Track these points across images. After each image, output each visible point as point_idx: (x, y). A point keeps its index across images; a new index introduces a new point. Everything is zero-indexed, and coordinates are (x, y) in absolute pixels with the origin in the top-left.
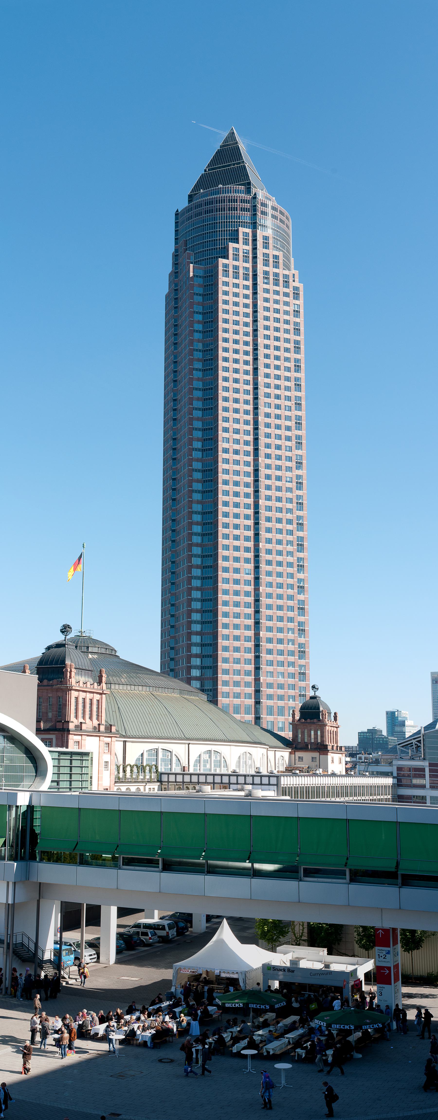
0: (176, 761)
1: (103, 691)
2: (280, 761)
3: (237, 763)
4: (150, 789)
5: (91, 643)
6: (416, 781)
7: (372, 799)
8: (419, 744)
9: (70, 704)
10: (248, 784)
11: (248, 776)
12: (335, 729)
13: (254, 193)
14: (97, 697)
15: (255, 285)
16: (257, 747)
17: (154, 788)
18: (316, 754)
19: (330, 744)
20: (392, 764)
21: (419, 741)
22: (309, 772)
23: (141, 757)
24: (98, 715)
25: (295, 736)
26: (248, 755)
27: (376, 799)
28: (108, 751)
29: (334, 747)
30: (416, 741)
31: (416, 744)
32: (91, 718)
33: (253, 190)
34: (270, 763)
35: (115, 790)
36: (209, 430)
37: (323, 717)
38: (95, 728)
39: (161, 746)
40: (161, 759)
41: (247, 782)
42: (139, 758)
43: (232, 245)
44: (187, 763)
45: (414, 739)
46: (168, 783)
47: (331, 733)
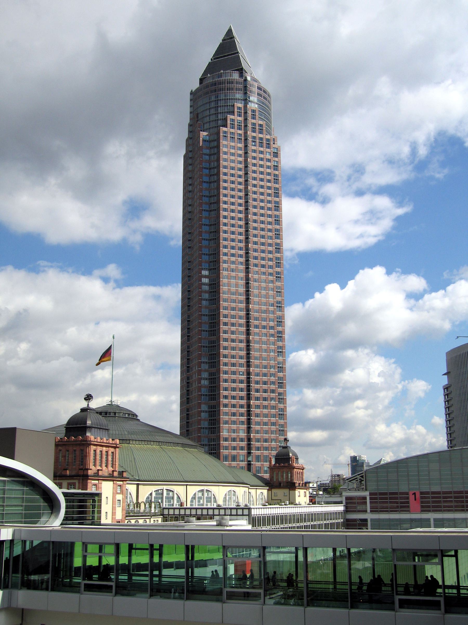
0: (177, 499)
1: (116, 445)
2: (260, 496)
3: (224, 498)
4: (154, 520)
5: (117, 410)
6: (359, 508)
7: (291, 527)
8: (362, 479)
9: (90, 456)
10: (227, 515)
11: (227, 508)
14: (112, 450)
15: (246, 146)
16: (219, 486)
17: (157, 520)
18: (286, 491)
19: (297, 482)
20: (342, 495)
21: (362, 477)
22: (279, 502)
23: (150, 496)
24: (113, 464)
25: (271, 477)
26: (233, 492)
27: (295, 526)
28: (120, 492)
29: (300, 484)
30: (360, 476)
31: (359, 479)
32: (107, 466)
33: (245, 74)
34: (253, 498)
35: (126, 523)
37: (292, 462)
38: (110, 474)
39: (165, 487)
40: (166, 497)
41: (227, 514)
42: (149, 497)
43: (230, 117)
44: (185, 500)
45: (358, 475)
46: (168, 516)
47: (298, 474)
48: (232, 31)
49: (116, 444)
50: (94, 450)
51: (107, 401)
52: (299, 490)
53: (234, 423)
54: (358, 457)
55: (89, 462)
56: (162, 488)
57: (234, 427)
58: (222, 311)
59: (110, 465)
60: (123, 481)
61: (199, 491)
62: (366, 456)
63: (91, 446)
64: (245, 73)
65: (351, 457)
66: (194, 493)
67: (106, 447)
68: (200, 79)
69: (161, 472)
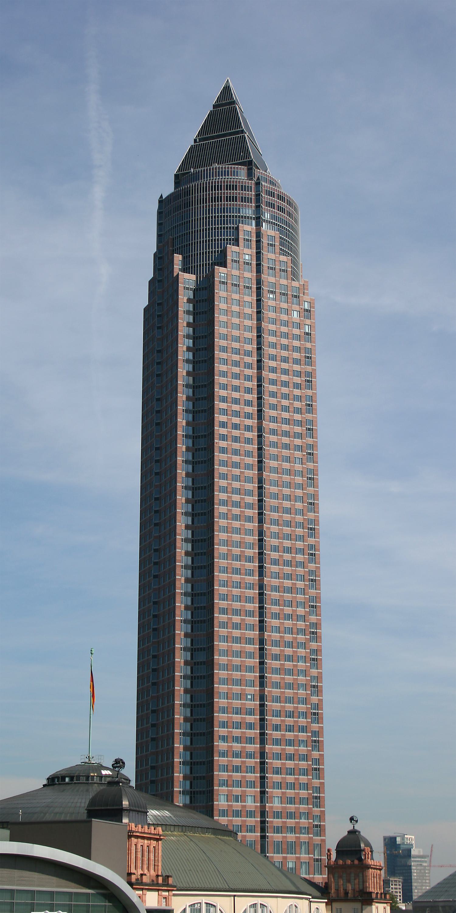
1: (160, 837)
9: (131, 853)
12: (378, 871)
13: (256, 178)
14: (154, 843)
16: (277, 897)
18: (358, 905)
36: (202, 489)
39: (204, 900)
48: (230, 90)
49: (159, 834)
50: (135, 845)
51: (83, 757)
52: (377, 904)
53: (239, 784)
54: (398, 840)
55: (130, 863)
56: (201, 901)
57: (237, 791)
58: (217, 588)
59: (152, 867)
60: (168, 891)
61: (251, 906)
62: (413, 837)
63: (132, 839)
64: (256, 170)
65: (385, 839)
66: (184, 908)
67: (148, 840)
68: (175, 175)
69: (196, 876)
